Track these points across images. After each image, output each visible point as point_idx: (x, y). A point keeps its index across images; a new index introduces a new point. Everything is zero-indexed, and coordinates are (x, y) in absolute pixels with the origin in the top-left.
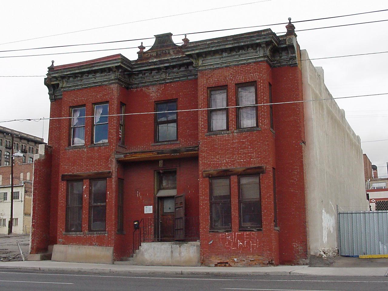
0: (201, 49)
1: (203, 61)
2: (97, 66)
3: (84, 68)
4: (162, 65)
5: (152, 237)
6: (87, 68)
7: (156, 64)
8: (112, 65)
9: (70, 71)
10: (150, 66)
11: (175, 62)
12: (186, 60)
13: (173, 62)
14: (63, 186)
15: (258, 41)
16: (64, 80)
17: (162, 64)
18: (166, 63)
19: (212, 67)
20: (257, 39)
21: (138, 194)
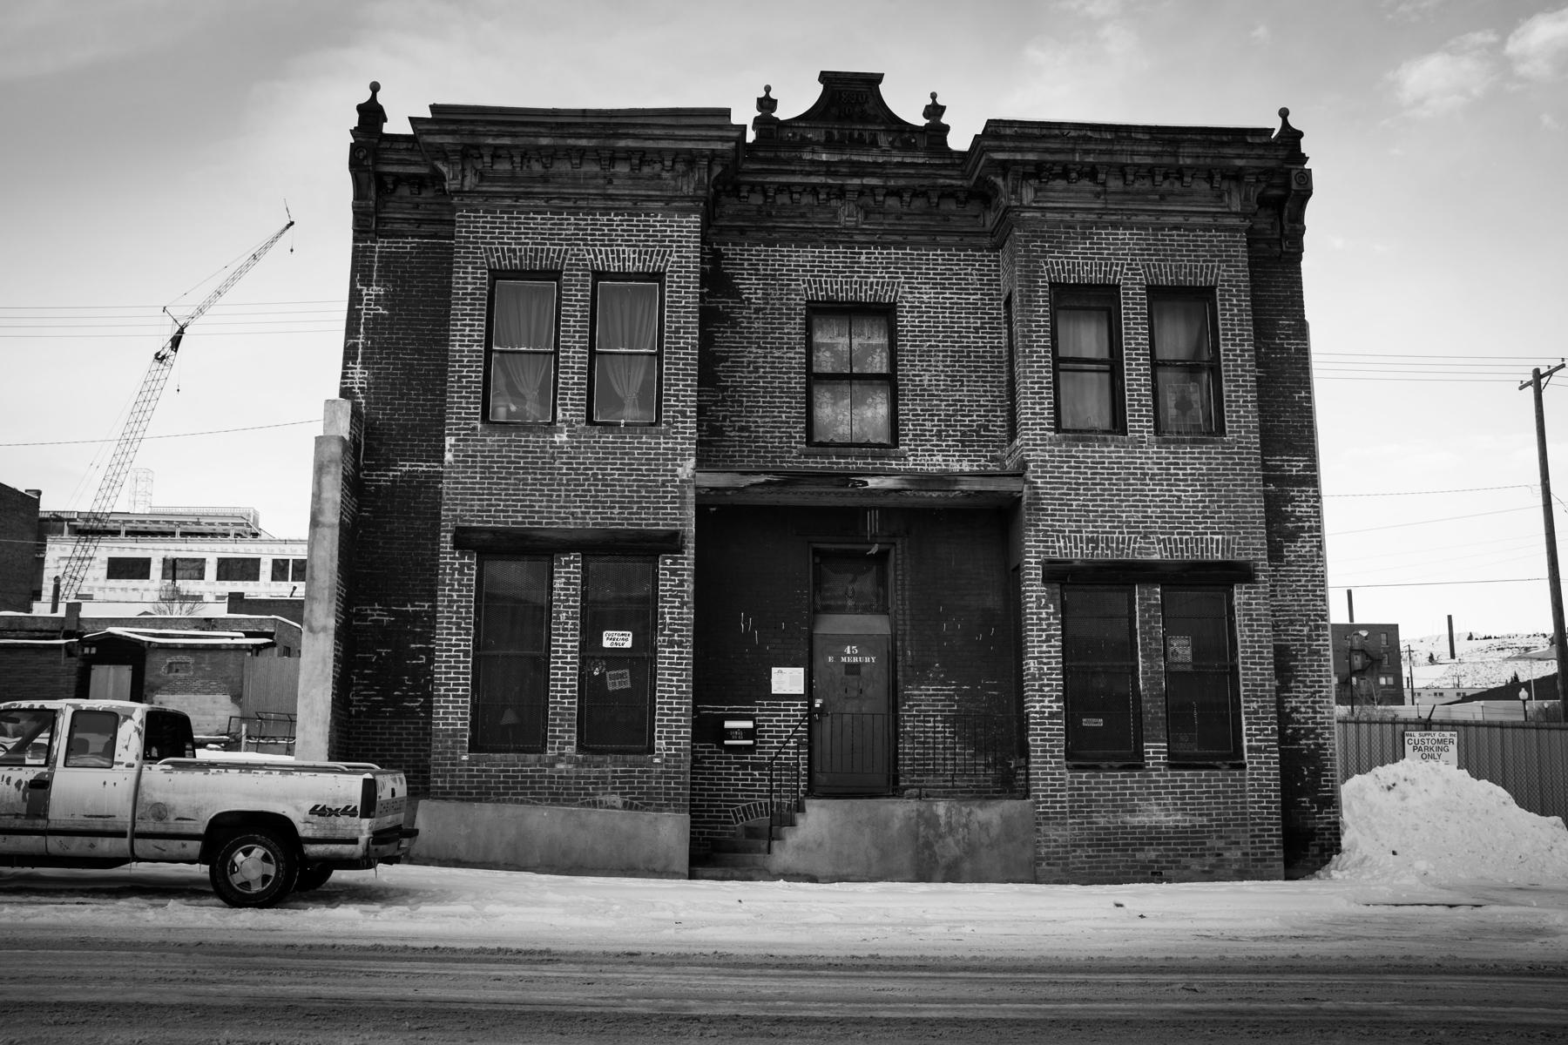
0: (1047, 150)
1: (1036, 191)
2: (635, 137)
3: (580, 136)
4: (857, 181)
5: (1279, 866)
6: (589, 137)
7: (835, 174)
8: (701, 145)
9: (513, 135)
10: (809, 174)
11: (906, 176)
12: (946, 177)
13: (897, 176)
14: (457, 579)
15: (1239, 163)
16: (468, 167)
17: (855, 175)
18: (873, 175)
19: (1067, 217)
20: (1239, 156)
21: (746, 620)
